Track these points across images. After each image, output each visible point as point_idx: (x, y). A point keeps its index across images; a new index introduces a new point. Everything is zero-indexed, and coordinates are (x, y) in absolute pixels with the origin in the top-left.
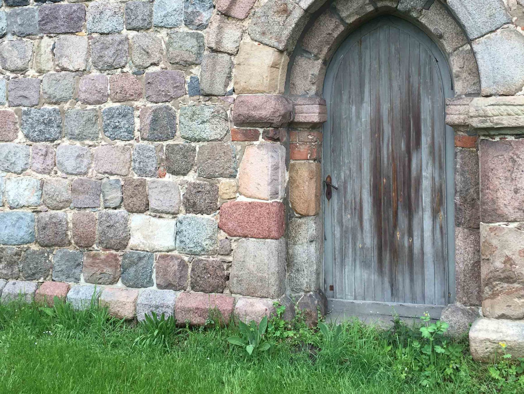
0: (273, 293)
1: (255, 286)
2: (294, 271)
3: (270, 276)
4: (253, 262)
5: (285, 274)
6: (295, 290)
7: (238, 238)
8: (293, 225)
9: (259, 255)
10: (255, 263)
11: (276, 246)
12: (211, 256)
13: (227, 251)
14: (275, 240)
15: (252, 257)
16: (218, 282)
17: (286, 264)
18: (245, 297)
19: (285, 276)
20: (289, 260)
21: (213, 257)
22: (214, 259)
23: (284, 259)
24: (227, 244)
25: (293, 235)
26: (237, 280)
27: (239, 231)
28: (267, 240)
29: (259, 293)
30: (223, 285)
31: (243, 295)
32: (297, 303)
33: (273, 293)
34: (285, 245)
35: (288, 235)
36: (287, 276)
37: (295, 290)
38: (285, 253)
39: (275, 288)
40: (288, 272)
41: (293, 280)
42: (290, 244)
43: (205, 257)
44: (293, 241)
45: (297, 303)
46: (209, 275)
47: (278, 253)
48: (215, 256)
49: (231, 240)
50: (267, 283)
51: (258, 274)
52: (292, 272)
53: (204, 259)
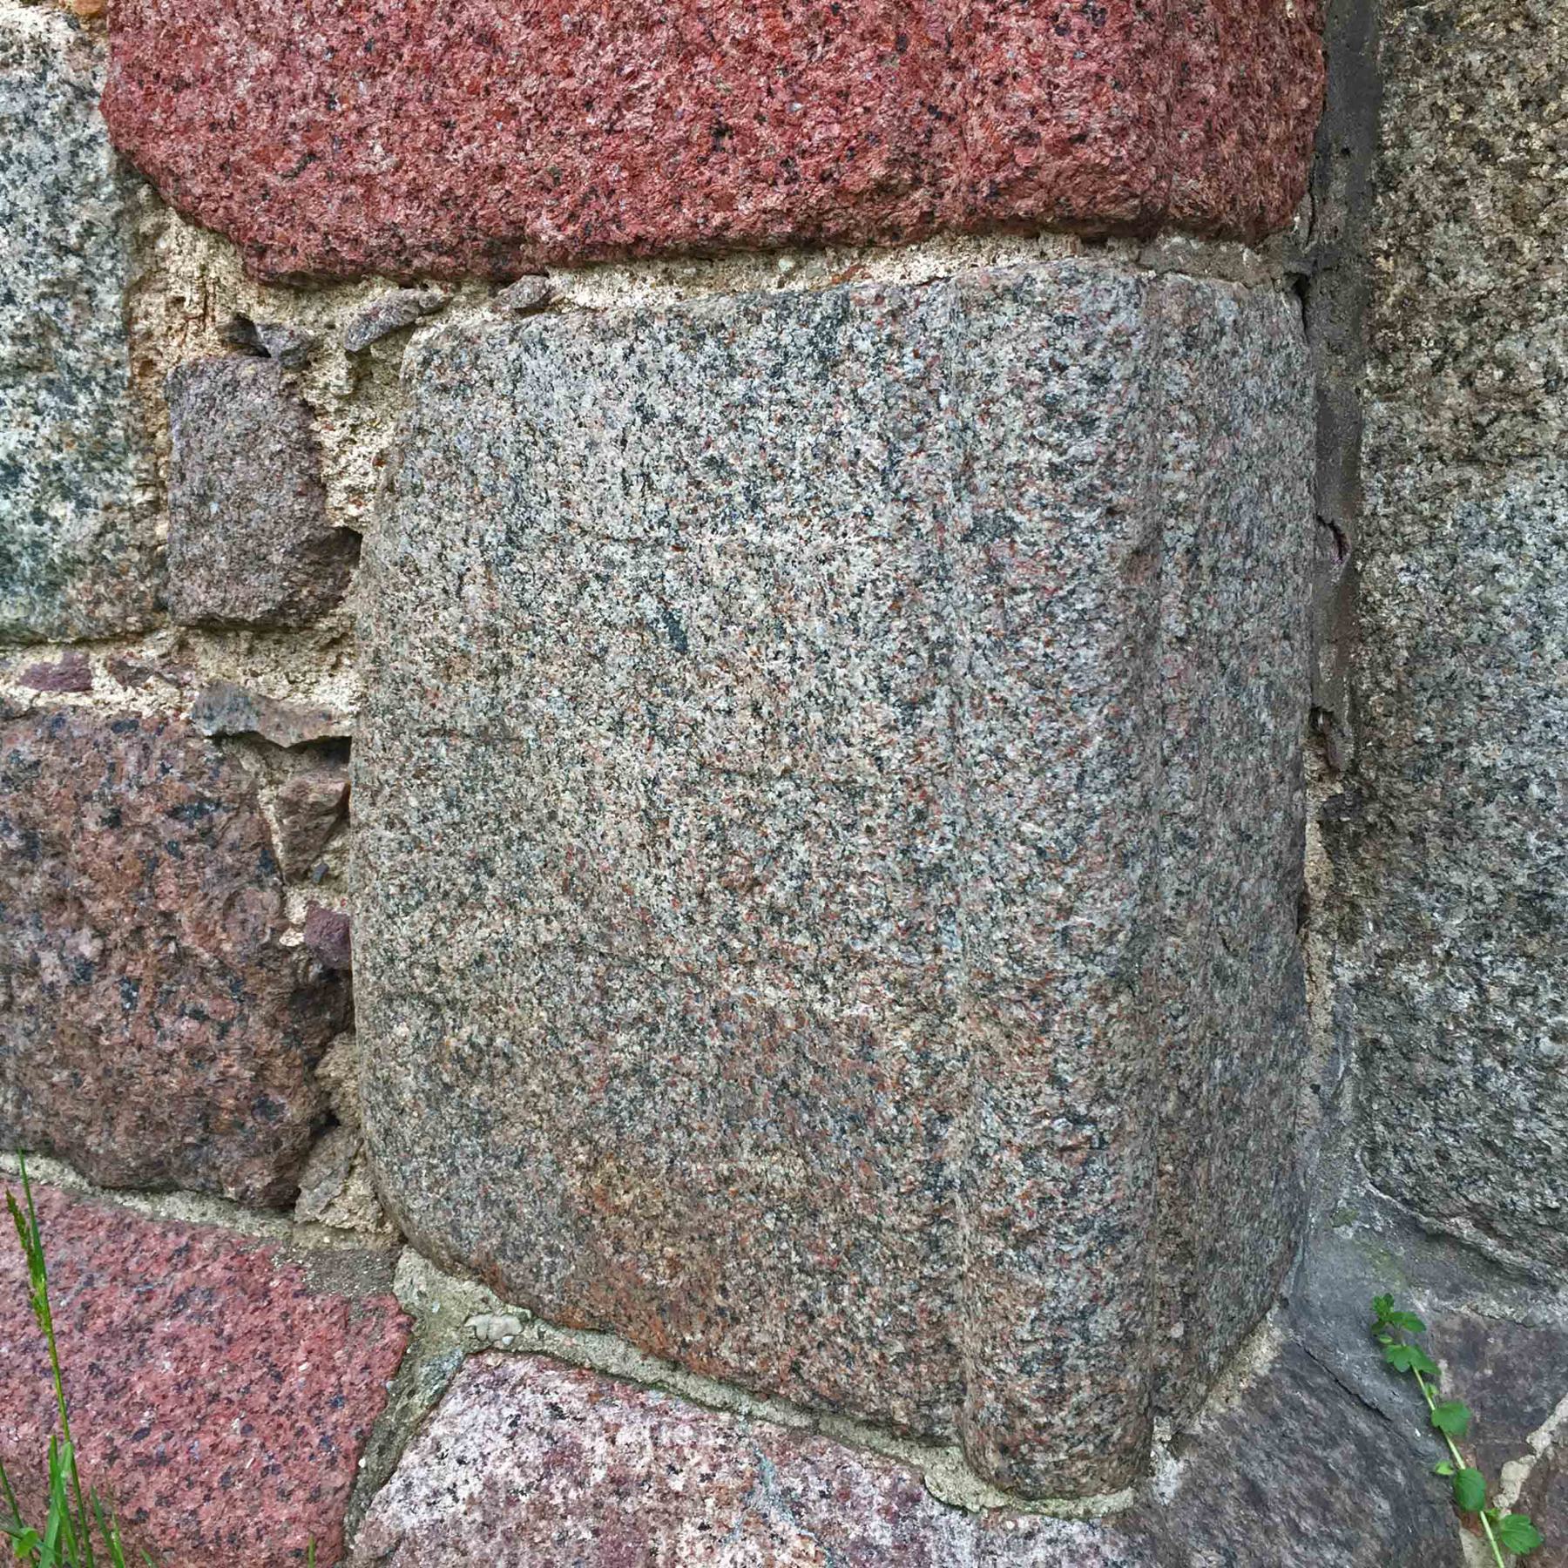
0: (1024, 1389)
1: (697, 1196)
2: (1454, 926)
3: (964, 1030)
4: (630, 757)
5: (1296, 975)
6: (1465, 1228)
7: (382, 296)
8: (1471, 96)
9: (729, 596)
10: (667, 763)
11: (1071, 387)
12: (97, 660)
13: (261, 562)
14: (1062, 254)
15: (622, 652)
16: (198, 1055)
17: (1314, 801)
18: (559, 1340)
19: (1289, 1011)
20: (1362, 720)
21: (128, 676)
22: (144, 705)
23: (1280, 704)
24: (251, 437)
25: (1477, 279)
26: (431, 1047)
27: (375, 157)
28: (883, 271)
29: (767, 1330)
30: (265, 1108)
31: (535, 1313)
32: (1516, 1473)
33: (1024, 1389)
34: (1300, 439)
35: (1367, 298)
36: (1322, 996)
37: (1465, 1228)
38: (1300, 595)
39: (1070, 1287)
40: (1350, 935)
41: (1425, 1069)
42: (1392, 454)
43: (38, 678)
44: (1456, 397)
45: (1516, 1473)
46: (88, 948)
47: (1142, 556)
48: (149, 652)
49: (306, 356)
50: (908, 1167)
51: (733, 985)
52: (1420, 938)
53: (25, 696)
